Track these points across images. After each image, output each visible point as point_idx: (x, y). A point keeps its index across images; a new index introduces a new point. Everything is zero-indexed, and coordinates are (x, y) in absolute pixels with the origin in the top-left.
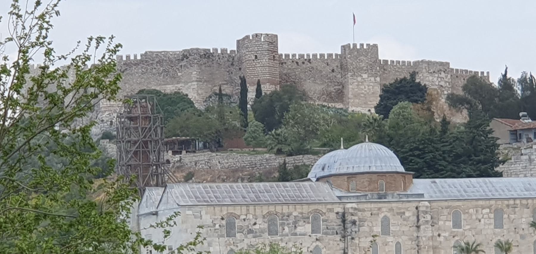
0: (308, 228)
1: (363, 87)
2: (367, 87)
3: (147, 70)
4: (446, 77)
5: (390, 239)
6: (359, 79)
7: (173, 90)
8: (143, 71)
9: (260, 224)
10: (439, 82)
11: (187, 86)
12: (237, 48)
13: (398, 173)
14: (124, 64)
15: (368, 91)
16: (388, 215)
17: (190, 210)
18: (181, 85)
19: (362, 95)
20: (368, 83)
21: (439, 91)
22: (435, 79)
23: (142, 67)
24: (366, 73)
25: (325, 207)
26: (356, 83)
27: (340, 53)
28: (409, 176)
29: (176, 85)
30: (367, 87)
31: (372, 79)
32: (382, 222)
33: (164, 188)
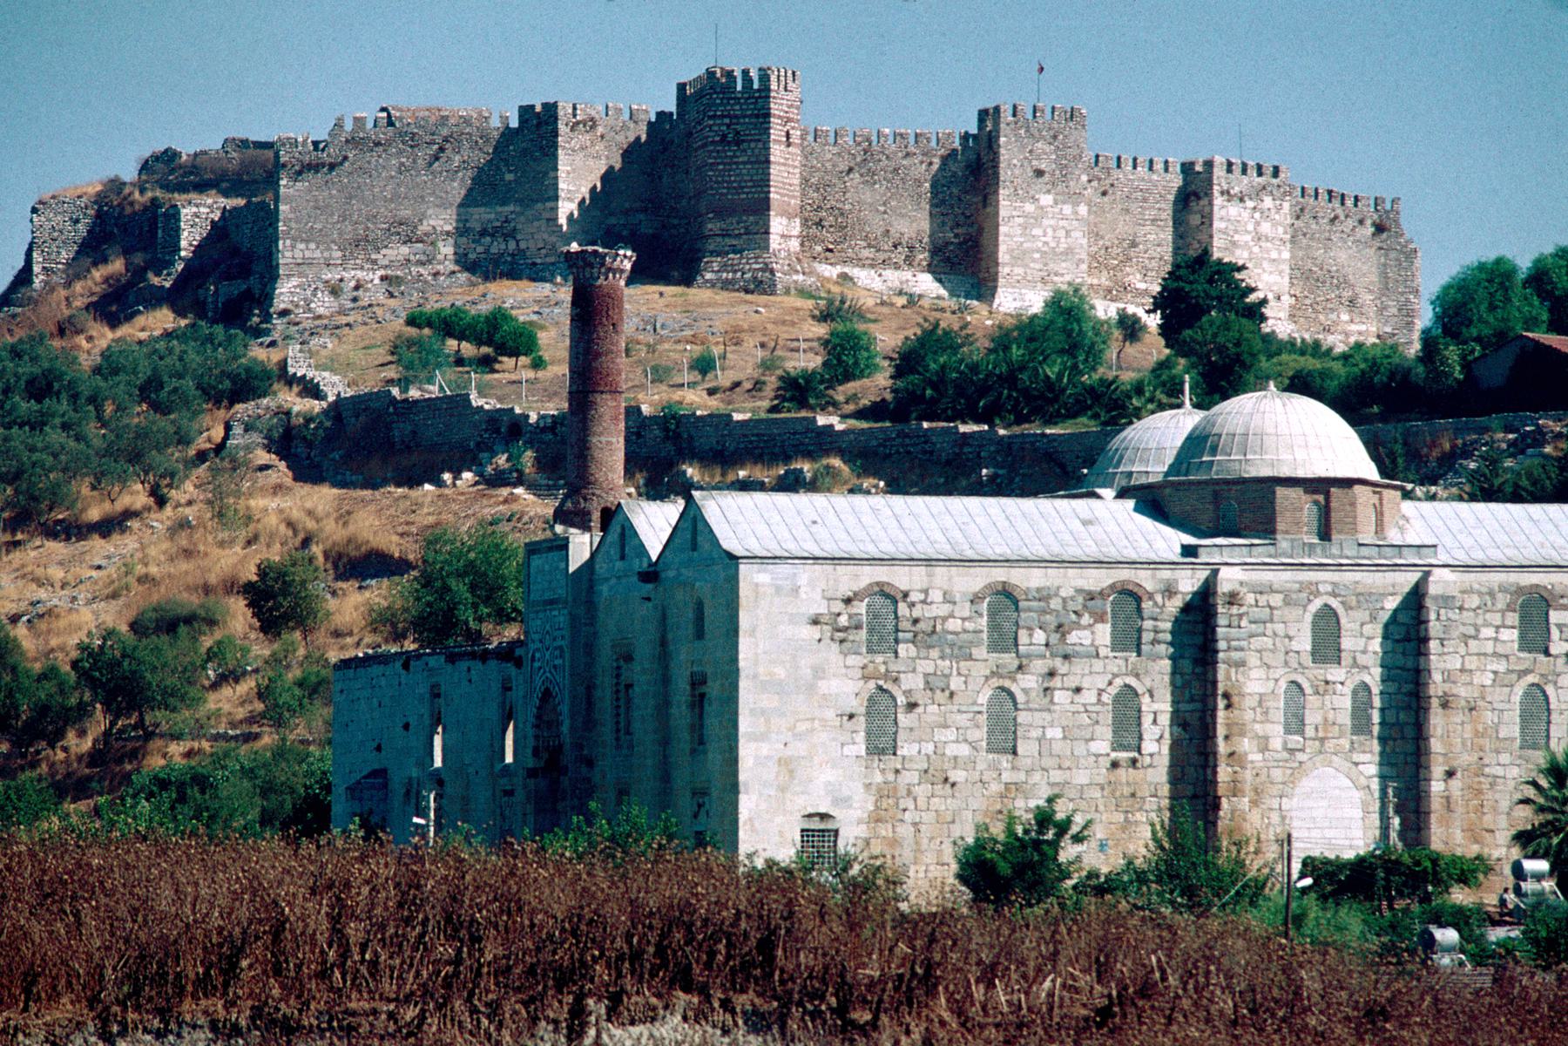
0: (1104, 632)
1: (1036, 231)
2: (1050, 231)
3: (414, 161)
4: (1279, 209)
5: (1335, 673)
6: (1029, 207)
7: (489, 221)
8: (402, 164)
9: (964, 619)
10: (1258, 224)
11: (529, 213)
12: (678, 105)
13: (701, 488)
14: (347, 141)
15: (1053, 244)
16: (1334, 603)
17: (765, 571)
18: (511, 208)
19: (1037, 256)
20: (1052, 222)
21: (1256, 249)
22: (1246, 214)
23: (400, 152)
24: (1049, 192)
25: (1153, 577)
26: (1021, 220)
27: (975, 131)
28: (1392, 492)
29: (499, 209)
30: (1050, 231)
31: (1067, 209)
32: (1314, 624)
33: (1281, 492)
